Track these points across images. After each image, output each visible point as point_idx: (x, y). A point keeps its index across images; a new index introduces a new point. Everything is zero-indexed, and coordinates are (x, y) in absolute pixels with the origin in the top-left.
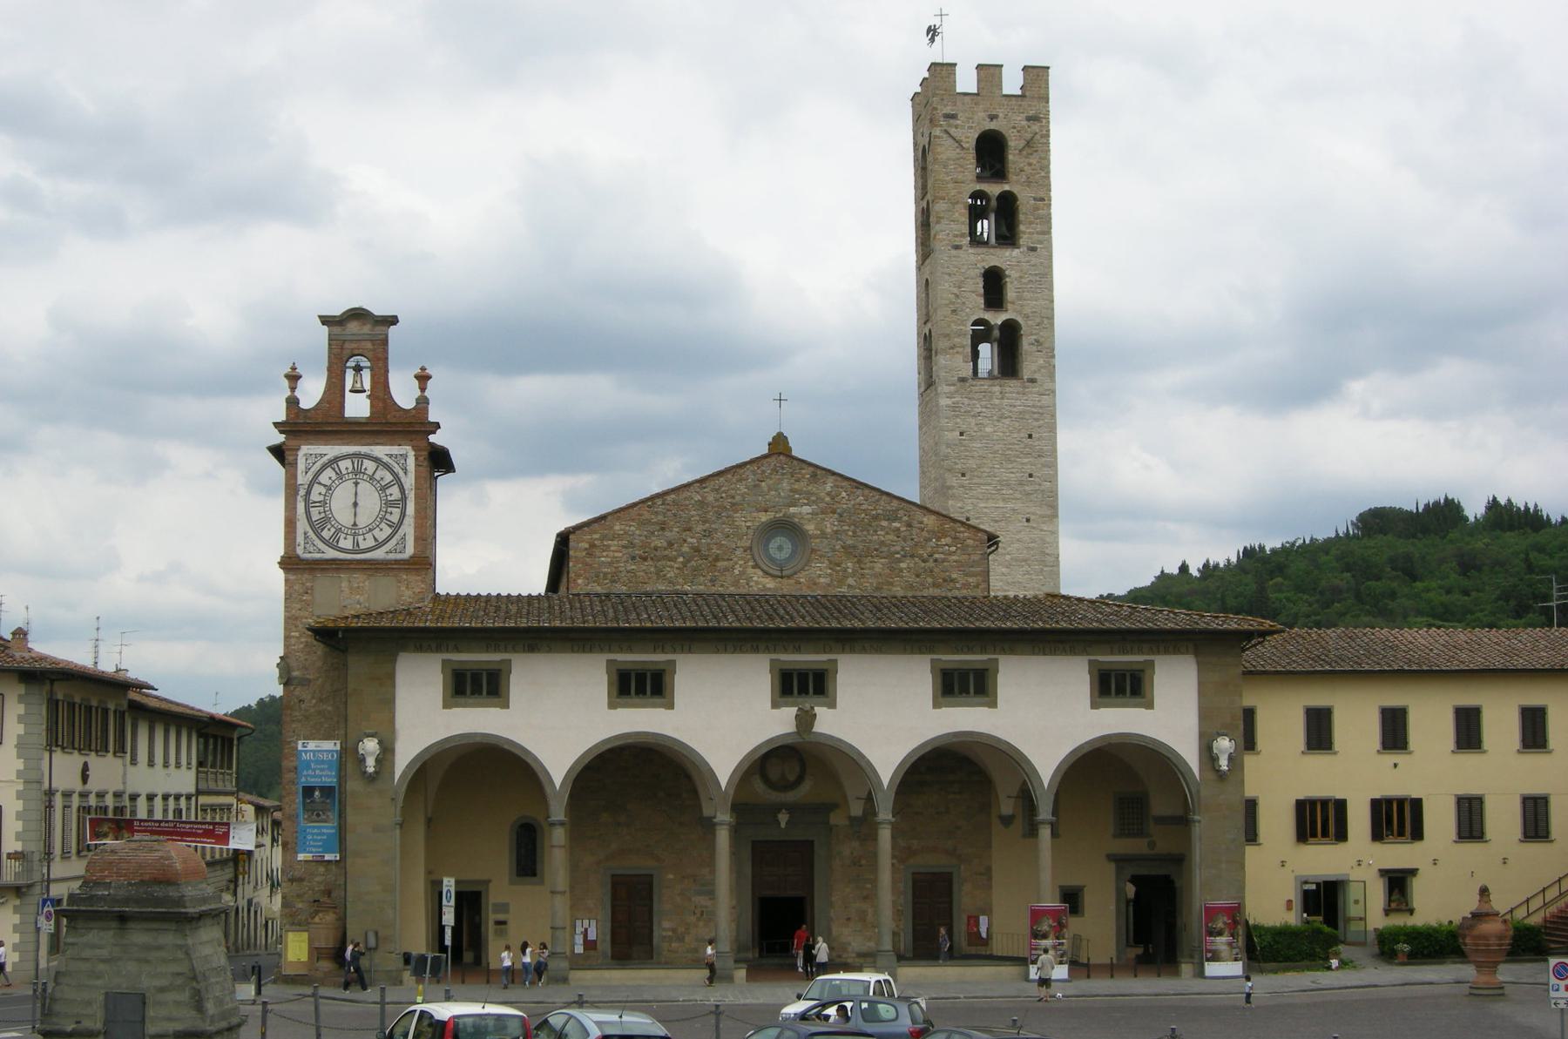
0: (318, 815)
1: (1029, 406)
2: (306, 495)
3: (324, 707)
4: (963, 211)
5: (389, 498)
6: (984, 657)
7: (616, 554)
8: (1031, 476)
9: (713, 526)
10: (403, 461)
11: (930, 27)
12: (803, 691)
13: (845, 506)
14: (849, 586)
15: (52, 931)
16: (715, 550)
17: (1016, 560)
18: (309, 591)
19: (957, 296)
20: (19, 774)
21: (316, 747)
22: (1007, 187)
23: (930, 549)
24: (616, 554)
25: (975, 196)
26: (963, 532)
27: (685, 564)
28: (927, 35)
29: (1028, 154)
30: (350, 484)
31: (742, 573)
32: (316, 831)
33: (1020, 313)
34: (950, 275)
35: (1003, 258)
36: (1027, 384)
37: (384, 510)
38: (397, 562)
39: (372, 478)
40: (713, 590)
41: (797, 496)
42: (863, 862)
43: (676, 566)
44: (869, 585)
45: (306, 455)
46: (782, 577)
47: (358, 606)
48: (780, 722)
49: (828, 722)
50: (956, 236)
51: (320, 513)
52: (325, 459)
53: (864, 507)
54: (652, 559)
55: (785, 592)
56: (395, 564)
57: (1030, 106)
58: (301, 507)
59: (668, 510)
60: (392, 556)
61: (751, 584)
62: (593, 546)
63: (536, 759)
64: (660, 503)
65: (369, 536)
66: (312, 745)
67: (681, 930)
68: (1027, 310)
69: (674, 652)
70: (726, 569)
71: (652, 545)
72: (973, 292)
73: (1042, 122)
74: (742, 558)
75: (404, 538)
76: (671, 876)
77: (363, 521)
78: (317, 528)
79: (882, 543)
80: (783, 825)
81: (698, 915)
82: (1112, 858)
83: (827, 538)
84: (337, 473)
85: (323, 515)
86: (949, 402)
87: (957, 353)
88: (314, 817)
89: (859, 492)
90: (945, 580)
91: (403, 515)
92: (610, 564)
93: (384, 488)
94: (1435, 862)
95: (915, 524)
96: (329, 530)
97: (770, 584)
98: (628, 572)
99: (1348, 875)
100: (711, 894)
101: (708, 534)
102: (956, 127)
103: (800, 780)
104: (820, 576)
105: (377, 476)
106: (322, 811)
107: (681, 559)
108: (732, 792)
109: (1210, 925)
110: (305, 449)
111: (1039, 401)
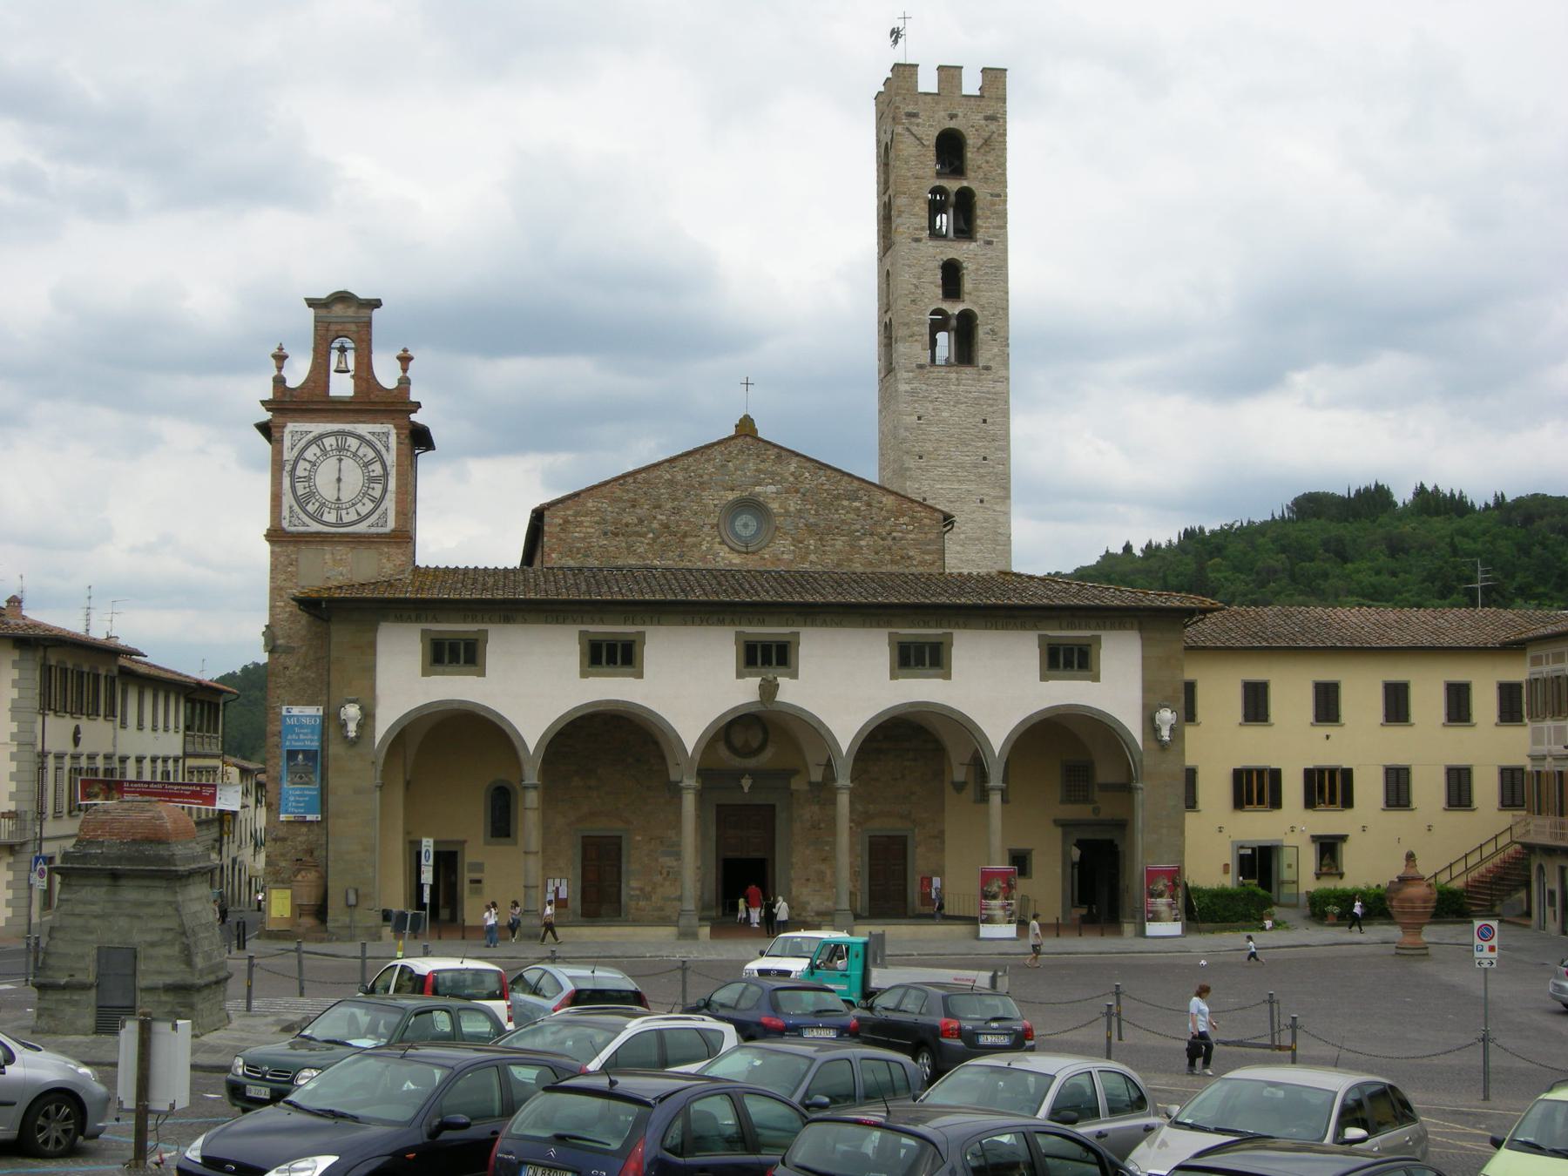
0: (301, 778)
1: (983, 392)
2: (291, 471)
3: (308, 674)
4: (923, 205)
5: (372, 474)
6: (940, 631)
7: (589, 530)
8: (985, 459)
9: (682, 503)
10: (385, 439)
11: (894, 29)
12: (767, 662)
13: (808, 486)
14: (811, 562)
15: (45, 888)
16: (684, 528)
17: (970, 539)
18: (294, 563)
19: (916, 287)
20: (13, 736)
21: (300, 712)
22: (965, 184)
23: (888, 528)
24: (589, 530)
25: (934, 191)
26: (920, 512)
27: (654, 540)
28: (891, 37)
29: (986, 152)
30: (334, 461)
31: (709, 549)
32: (298, 793)
33: (975, 303)
34: (910, 266)
35: (960, 251)
36: (982, 371)
37: (367, 485)
38: (379, 535)
39: (355, 454)
40: (682, 565)
41: (762, 476)
42: (822, 825)
43: (646, 541)
44: (830, 560)
45: (292, 432)
46: (747, 553)
47: (341, 578)
48: (744, 692)
49: (790, 692)
50: (916, 229)
51: (305, 488)
52: (310, 436)
53: (825, 487)
54: (623, 535)
55: (750, 567)
56: (377, 537)
57: (988, 106)
58: (286, 482)
59: (639, 488)
60: (374, 530)
61: (718, 559)
62: (566, 521)
63: (511, 725)
64: (631, 481)
65: (352, 510)
66: (296, 710)
67: (648, 889)
68: (983, 301)
69: (644, 623)
70: (694, 545)
71: (624, 521)
72: (931, 283)
73: (999, 122)
74: (709, 535)
75: (385, 512)
76: (638, 838)
77: (345, 497)
78: (302, 502)
79: (843, 522)
80: (746, 790)
81: (665, 875)
82: (1058, 823)
83: (790, 516)
84: (321, 449)
85: (308, 490)
86: (907, 387)
87: (916, 341)
88: (297, 779)
89: (822, 472)
90: (902, 558)
91: (385, 490)
92: (584, 539)
93: (366, 465)
94: (1364, 829)
95: (874, 503)
96: (313, 504)
97: (736, 560)
98: (600, 547)
99: (1282, 841)
100: (678, 855)
101: (676, 511)
102: (918, 125)
103: (761, 748)
104: (783, 553)
105: (360, 453)
106: (304, 773)
107: (651, 535)
108: (698, 758)
109: (1151, 887)
110: (291, 427)
111: (993, 388)
